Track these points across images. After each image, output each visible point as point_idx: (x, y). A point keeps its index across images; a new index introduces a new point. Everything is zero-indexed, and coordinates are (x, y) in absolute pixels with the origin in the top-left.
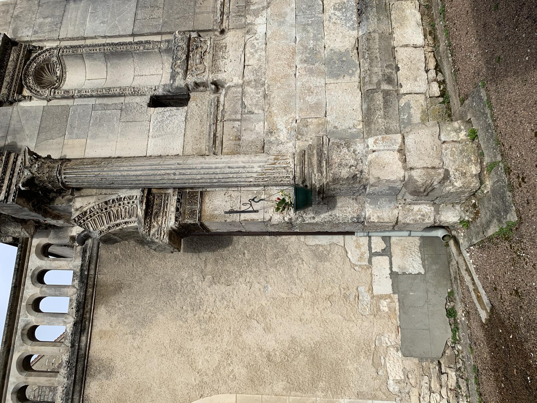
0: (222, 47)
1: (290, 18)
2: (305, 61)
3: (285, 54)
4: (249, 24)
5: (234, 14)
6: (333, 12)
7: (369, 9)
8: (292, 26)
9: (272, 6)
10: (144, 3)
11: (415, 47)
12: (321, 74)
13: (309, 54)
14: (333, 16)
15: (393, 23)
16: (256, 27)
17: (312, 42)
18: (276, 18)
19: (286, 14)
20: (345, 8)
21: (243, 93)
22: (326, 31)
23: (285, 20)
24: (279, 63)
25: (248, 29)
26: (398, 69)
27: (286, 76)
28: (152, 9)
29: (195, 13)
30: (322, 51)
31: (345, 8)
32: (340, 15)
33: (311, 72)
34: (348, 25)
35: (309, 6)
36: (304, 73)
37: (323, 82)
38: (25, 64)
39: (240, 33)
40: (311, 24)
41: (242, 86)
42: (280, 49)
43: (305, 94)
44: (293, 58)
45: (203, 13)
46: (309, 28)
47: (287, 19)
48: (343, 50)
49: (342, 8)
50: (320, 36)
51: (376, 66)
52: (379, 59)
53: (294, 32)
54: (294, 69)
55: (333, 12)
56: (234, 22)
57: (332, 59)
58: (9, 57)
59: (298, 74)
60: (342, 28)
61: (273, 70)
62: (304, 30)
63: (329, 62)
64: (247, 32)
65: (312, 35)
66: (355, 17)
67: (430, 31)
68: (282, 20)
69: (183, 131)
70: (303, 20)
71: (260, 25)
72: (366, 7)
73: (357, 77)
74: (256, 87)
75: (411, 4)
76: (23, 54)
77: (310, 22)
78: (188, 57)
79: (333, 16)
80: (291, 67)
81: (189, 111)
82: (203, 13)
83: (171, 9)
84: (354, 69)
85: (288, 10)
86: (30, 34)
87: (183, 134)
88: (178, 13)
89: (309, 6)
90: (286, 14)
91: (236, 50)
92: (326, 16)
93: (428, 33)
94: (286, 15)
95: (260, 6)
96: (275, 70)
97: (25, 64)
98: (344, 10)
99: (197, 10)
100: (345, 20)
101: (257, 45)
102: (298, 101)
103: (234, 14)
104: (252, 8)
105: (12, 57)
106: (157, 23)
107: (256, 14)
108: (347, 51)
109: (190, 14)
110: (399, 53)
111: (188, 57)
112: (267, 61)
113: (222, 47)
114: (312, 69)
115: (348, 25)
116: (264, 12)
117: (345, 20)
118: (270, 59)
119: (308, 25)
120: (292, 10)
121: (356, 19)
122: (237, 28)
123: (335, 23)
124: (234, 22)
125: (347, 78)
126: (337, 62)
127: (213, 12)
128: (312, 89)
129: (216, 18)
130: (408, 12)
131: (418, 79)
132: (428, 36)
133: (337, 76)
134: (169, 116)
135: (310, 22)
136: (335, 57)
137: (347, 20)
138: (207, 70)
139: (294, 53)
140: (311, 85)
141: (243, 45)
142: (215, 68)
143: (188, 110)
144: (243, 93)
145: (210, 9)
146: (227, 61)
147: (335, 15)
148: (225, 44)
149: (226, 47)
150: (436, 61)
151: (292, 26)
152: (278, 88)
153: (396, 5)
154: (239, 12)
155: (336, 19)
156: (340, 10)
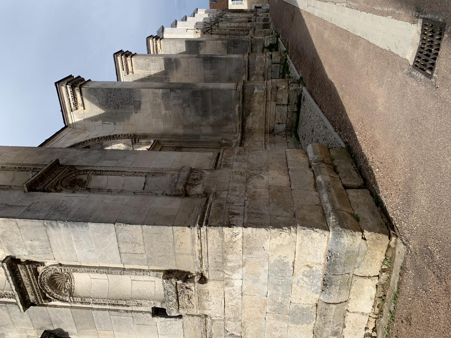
0: (205, 293)
1: (264, 277)
2: (274, 311)
3: (257, 304)
4: (226, 278)
5: (212, 269)
6: (301, 277)
7: (333, 286)
8: (264, 284)
9: (247, 266)
10: (124, 239)
11: (363, 313)
12: (285, 320)
13: (277, 306)
14: (301, 281)
15: (351, 295)
16: (233, 281)
17: (280, 298)
18: (250, 276)
19: (260, 274)
20: (313, 276)
21: (225, 324)
22: (293, 291)
23: (258, 278)
24: (253, 309)
25: (226, 282)
26: (344, 327)
27: (259, 318)
28: (134, 245)
29: (175, 254)
30: (288, 306)
31: (313, 276)
32: (307, 281)
33: (278, 318)
34: (313, 289)
35: (281, 270)
36: (273, 318)
37: (286, 325)
38: (37, 279)
39: (219, 284)
40: (281, 285)
41: (224, 321)
42: (254, 300)
43: (272, 330)
44: (264, 307)
45: (183, 254)
46: (279, 288)
47: (261, 277)
48: (305, 306)
49: (310, 275)
50: (288, 294)
51: (328, 327)
52: (332, 322)
53: (266, 289)
54: (265, 315)
55: (301, 277)
56: (213, 275)
57: (295, 312)
58: (20, 273)
59: (267, 318)
60: (307, 291)
61: (248, 313)
62: (275, 288)
63: (292, 314)
64: (226, 284)
65: (281, 293)
66: (320, 284)
67: (379, 304)
68: (256, 278)
69: (182, 333)
70: (274, 280)
71: (237, 279)
72: (331, 285)
73: (313, 326)
74: (234, 321)
75: (371, 283)
76: (31, 272)
77: (280, 283)
78: (178, 300)
79: (301, 281)
80: (262, 313)
81: (185, 323)
82: (183, 254)
83: (152, 247)
84: (311, 320)
85: (262, 271)
86: (26, 254)
87: (183, 335)
88: (159, 252)
89: (281, 270)
90: (260, 274)
91: (217, 297)
92: (295, 280)
93: (377, 305)
94: (260, 274)
95: (236, 264)
96: (250, 314)
97: (37, 279)
98: (311, 277)
99: (177, 251)
100: (311, 285)
101: (235, 295)
102: (266, 334)
103: (212, 269)
104: (229, 264)
105: (22, 274)
106: (142, 258)
107: (233, 270)
108: (308, 308)
109: (171, 253)
110: (349, 317)
111: (178, 300)
112: (243, 307)
113: (205, 293)
114: (278, 317)
115: (313, 289)
116: (240, 270)
117: (311, 285)
118: (245, 306)
119: (279, 285)
120: (265, 271)
121: (320, 285)
122: (217, 280)
123: (302, 287)
124: (213, 275)
125: (305, 325)
126: (299, 314)
127: (192, 254)
128: (277, 328)
129: (195, 260)
130: (366, 288)
131: (357, 334)
132: (376, 308)
133: (298, 323)
134: (170, 324)
135: (280, 283)
136: (297, 311)
137: (312, 285)
138: (195, 307)
139: (265, 304)
140: (277, 326)
141: (223, 293)
142: (200, 305)
143: (183, 322)
144: (225, 324)
145: (189, 251)
146: (211, 303)
147: (303, 280)
148: (207, 291)
149: (208, 293)
150: (376, 325)
151: (264, 284)
152: (252, 325)
153: (357, 281)
154: (217, 267)
155: (303, 283)
156: (307, 277)
